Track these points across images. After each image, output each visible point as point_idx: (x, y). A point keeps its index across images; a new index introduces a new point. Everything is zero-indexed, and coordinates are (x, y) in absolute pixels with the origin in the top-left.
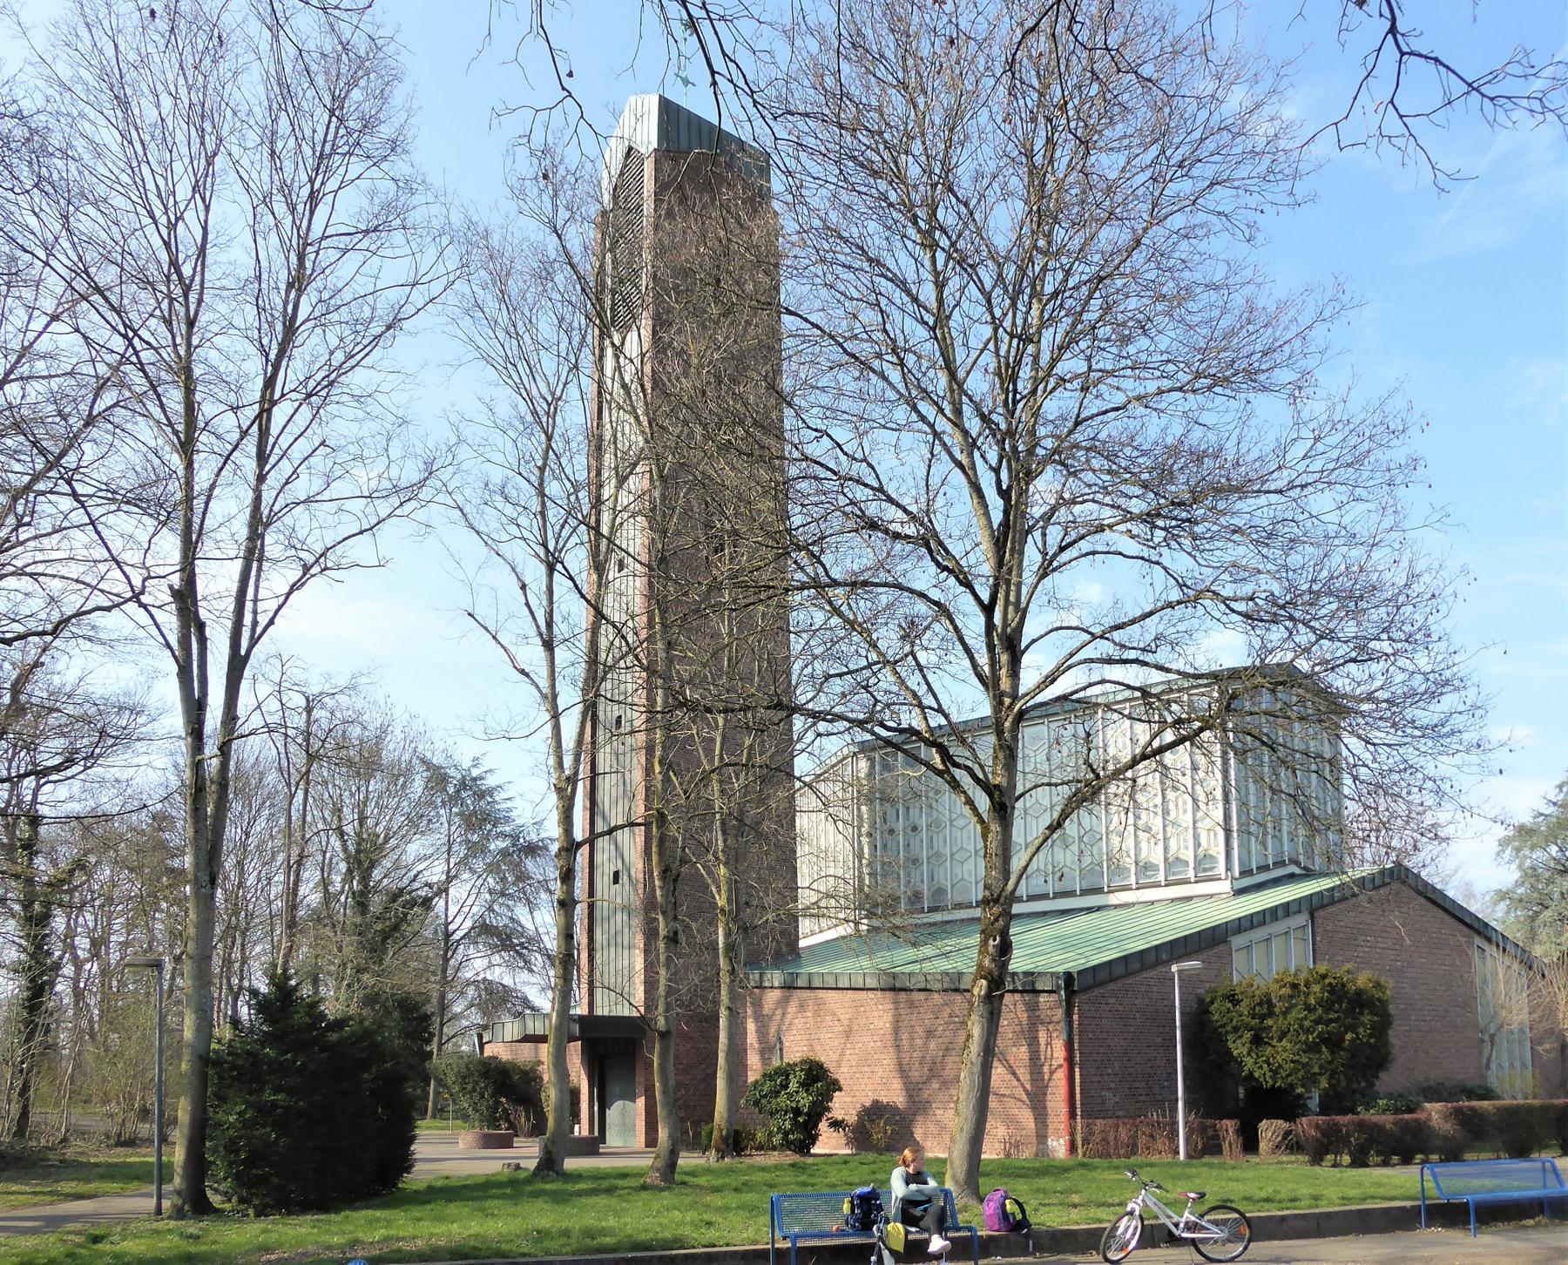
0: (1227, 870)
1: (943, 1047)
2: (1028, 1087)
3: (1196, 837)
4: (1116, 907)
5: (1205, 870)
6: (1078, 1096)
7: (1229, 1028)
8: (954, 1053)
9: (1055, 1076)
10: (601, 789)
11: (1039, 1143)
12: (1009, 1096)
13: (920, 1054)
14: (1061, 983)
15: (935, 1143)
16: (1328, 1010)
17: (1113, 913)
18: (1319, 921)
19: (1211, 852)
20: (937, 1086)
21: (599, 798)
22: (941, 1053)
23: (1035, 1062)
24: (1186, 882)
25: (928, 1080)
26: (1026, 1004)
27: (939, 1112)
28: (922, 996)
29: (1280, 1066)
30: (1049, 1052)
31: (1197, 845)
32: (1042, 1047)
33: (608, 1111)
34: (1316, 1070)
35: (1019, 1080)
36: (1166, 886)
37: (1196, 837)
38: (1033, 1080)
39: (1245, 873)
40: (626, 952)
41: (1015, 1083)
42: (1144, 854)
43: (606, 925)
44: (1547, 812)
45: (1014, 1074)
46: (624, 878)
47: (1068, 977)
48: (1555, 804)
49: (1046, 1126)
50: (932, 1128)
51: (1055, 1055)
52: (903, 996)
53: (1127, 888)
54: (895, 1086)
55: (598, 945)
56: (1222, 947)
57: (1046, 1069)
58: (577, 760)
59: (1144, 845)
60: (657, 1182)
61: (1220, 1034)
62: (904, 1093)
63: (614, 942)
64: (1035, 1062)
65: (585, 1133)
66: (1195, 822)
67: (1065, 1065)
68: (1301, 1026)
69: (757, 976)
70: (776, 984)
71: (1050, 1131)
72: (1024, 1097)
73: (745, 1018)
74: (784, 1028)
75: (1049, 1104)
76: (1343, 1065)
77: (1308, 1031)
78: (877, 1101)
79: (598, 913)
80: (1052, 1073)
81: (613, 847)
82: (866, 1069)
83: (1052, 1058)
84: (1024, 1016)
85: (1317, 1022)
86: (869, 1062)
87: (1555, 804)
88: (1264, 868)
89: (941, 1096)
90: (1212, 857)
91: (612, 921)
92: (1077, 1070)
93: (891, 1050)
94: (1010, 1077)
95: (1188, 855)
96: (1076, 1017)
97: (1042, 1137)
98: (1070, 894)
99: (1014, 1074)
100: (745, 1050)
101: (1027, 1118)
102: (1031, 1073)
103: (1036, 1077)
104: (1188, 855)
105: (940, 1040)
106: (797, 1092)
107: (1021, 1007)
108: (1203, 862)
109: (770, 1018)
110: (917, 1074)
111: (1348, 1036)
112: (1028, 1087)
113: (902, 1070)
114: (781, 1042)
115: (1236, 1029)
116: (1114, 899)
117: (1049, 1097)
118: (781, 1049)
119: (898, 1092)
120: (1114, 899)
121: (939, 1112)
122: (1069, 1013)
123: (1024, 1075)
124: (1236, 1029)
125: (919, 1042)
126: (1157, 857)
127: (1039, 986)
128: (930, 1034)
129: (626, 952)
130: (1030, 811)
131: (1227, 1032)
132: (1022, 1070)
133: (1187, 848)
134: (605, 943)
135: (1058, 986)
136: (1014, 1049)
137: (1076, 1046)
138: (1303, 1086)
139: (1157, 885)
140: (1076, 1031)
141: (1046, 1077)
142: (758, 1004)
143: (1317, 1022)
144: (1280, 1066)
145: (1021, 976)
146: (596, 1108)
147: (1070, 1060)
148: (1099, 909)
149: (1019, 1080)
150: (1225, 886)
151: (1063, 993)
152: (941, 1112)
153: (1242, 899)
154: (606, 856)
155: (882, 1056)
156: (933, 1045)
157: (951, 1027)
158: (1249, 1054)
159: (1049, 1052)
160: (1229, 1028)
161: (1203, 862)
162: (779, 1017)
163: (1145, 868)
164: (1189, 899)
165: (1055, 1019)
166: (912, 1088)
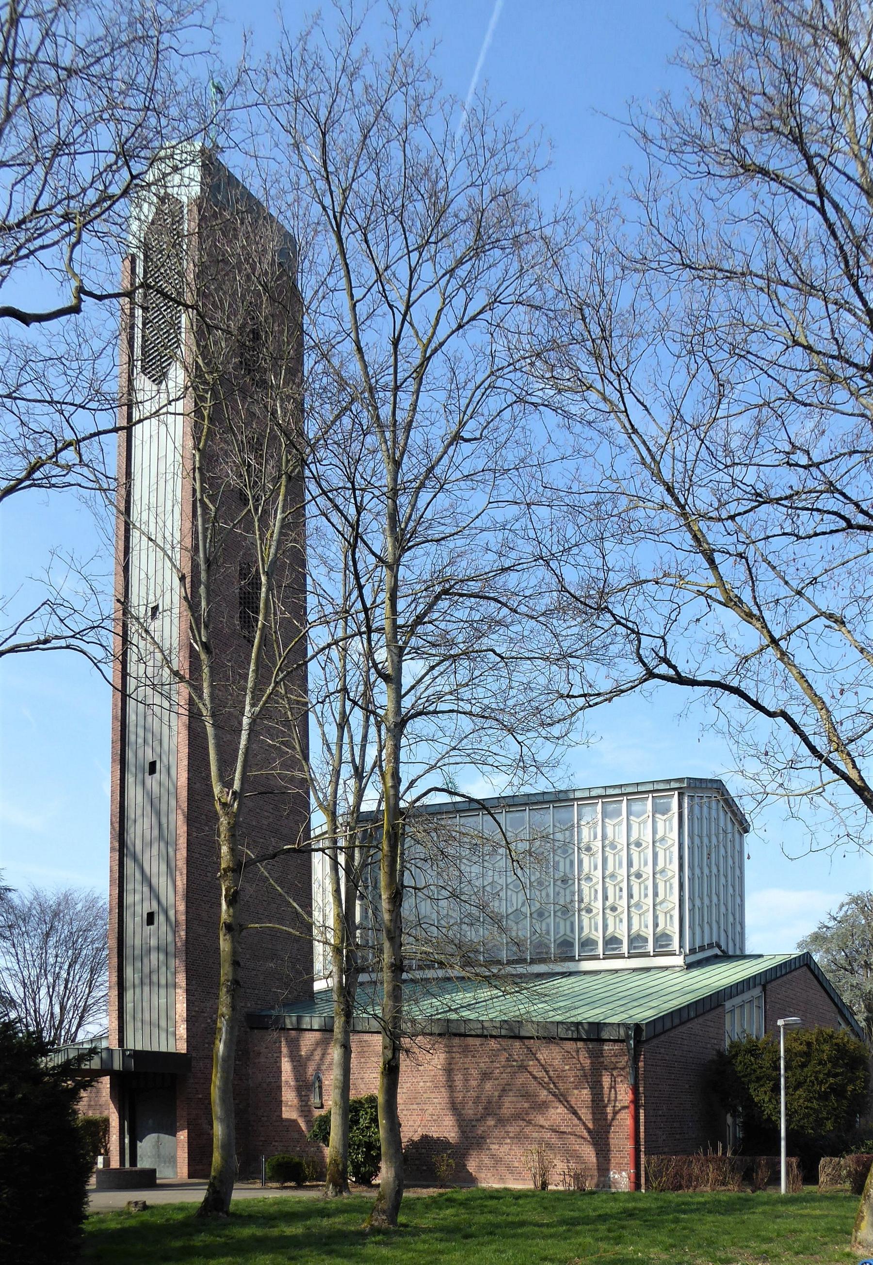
0: (681, 947)
1: (500, 1088)
2: (590, 1125)
3: (655, 917)
4: (586, 973)
5: (662, 946)
6: (642, 1135)
7: (753, 1077)
8: (511, 1094)
9: (618, 1117)
10: (131, 831)
11: (600, 1176)
12: (570, 1133)
13: (474, 1094)
14: (631, 1033)
15: (489, 1175)
16: (835, 1065)
17: (588, 978)
18: (768, 992)
19: (668, 932)
20: (493, 1123)
21: (129, 838)
22: (496, 1094)
23: (598, 1104)
24: (646, 955)
25: (483, 1118)
26: (589, 1051)
27: (493, 1147)
28: (478, 1041)
29: (796, 1111)
30: (613, 1095)
31: (656, 925)
32: (606, 1090)
33: (139, 1144)
34: (825, 1114)
35: (580, 1119)
36: (629, 957)
37: (655, 917)
38: (595, 1120)
39: (693, 951)
40: (163, 992)
41: (576, 1121)
42: (610, 930)
43: (138, 964)
44: (830, 925)
45: (575, 1113)
46: (160, 919)
47: (637, 1027)
48: (835, 919)
49: (607, 1160)
50: (487, 1161)
51: (619, 1098)
52: (456, 1041)
53: (596, 958)
54: (446, 1123)
55: (129, 983)
56: (720, 1009)
57: (609, 1110)
58: (365, 737)
59: (610, 922)
60: (385, 1225)
61: (743, 1083)
62: (456, 1129)
63: (147, 980)
64: (598, 1104)
65: (115, 1164)
66: (654, 905)
67: (632, 1107)
68: (817, 1079)
69: (294, 1019)
70: (316, 1027)
71: (612, 1165)
72: (586, 1134)
73: (280, 1057)
74: (324, 1067)
75: (612, 1141)
76: (845, 1112)
77: (821, 1083)
78: (427, 1136)
79: (128, 952)
80: (615, 1113)
81: (146, 889)
82: (415, 1107)
83: (615, 1100)
84: (587, 1063)
85: (828, 1075)
86: (419, 1101)
87: (835, 919)
88: (702, 948)
89: (496, 1133)
90: (667, 935)
91: (146, 961)
92: (642, 1111)
93: (443, 1090)
94: (570, 1116)
95: (649, 933)
96: (641, 1064)
97: (603, 1167)
98: (522, 961)
99: (575, 1113)
100: (279, 1088)
101: (589, 1154)
102: (593, 1113)
103: (599, 1116)
104: (649, 933)
105: (496, 1082)
106: (367, 1128)
107: (583, 1054)
108: (662, 940)
109: (309, 1057)
110: (471, 1112)
111: (850, 1088)
112: (590, 1125)
113: (455, 1108)
114: (320, 1081)
115: (758, 1079)
116: (587, 966)
117: (612, 1135)
118: (320, 1087)
119: (449, 1128)
120: (587, 966)
121: (493, 1147)
122: (635, 1060)
123: (586, 1114)
124: (758, 1079)
125: (474, 1083)
126: (622, 934)
127: (605, 1035)
128: (486, 1076)
129: (163, 992)
130: (511, 887)
131: (750, 1081)
132: (583, 1111)
133: (647, 927)
134: (137, 981)
135: (628, 1036)
136: (576, 1092)
137: (641, 1089)
138: (812, 1129)
139: (621, 956)
140: (641, 1077)
141: (609, 1117)
142: (294, 1046)
143: (828, 1075)
144: (796, 1111)
145: (586, 1027)
146: (127, 1141)
147: (636, 1101)
148: (570, 974)
149: (580, 1119)
150: (679, 961)
151: (632, 1042)
152: (496, 1147)
153: (695, 973)
154: (138, 897)
155: (433, 1095)
156: (488, 1086)
157: (509, 1070)
158: (770, 1101)
159: (613, 1095)
160: (753, 1077)
161: (662, 940)
162: (317, 1058)
163: (612, 942)
164: (647, 969)
165: (620, 1065)
166: (465, 1125)
